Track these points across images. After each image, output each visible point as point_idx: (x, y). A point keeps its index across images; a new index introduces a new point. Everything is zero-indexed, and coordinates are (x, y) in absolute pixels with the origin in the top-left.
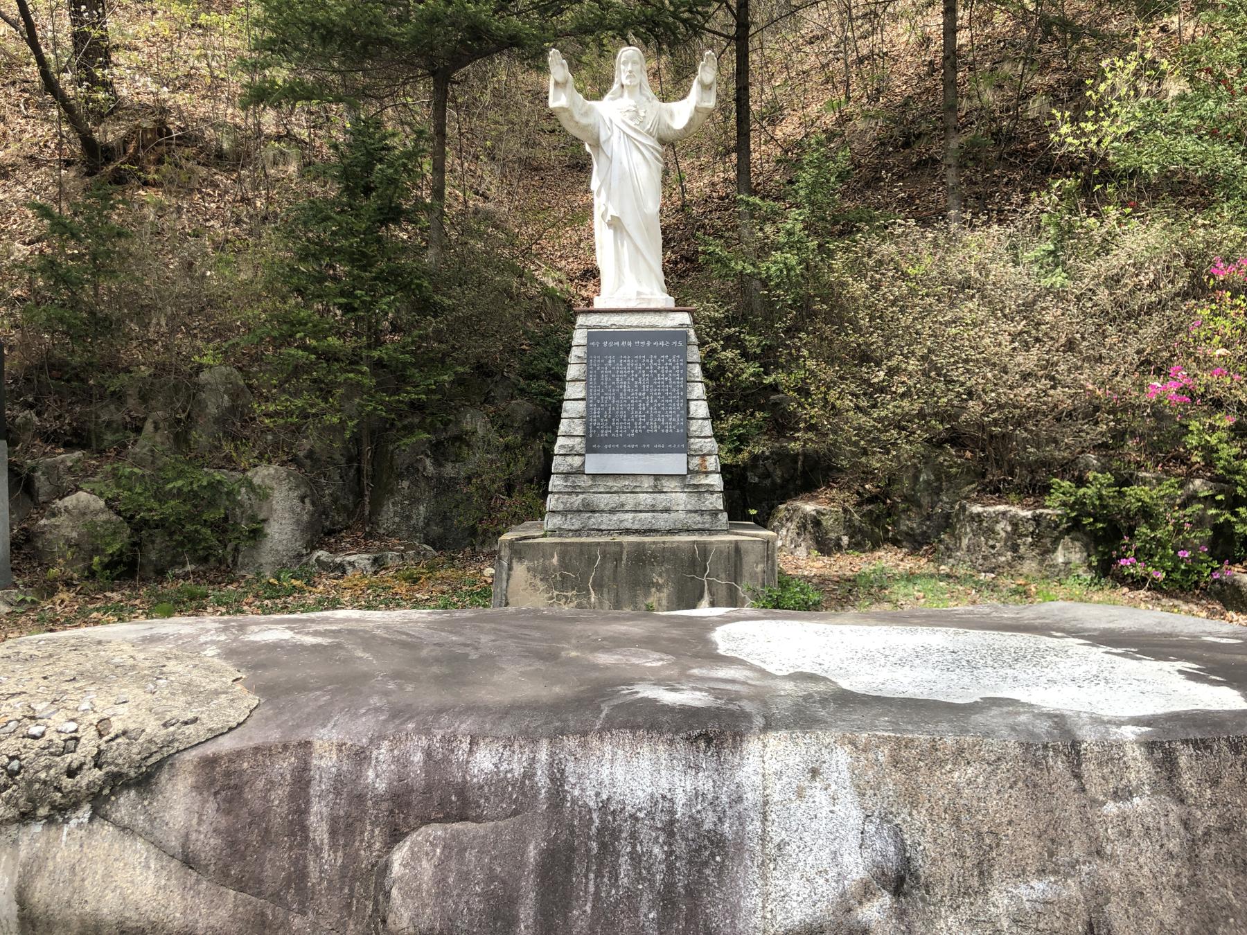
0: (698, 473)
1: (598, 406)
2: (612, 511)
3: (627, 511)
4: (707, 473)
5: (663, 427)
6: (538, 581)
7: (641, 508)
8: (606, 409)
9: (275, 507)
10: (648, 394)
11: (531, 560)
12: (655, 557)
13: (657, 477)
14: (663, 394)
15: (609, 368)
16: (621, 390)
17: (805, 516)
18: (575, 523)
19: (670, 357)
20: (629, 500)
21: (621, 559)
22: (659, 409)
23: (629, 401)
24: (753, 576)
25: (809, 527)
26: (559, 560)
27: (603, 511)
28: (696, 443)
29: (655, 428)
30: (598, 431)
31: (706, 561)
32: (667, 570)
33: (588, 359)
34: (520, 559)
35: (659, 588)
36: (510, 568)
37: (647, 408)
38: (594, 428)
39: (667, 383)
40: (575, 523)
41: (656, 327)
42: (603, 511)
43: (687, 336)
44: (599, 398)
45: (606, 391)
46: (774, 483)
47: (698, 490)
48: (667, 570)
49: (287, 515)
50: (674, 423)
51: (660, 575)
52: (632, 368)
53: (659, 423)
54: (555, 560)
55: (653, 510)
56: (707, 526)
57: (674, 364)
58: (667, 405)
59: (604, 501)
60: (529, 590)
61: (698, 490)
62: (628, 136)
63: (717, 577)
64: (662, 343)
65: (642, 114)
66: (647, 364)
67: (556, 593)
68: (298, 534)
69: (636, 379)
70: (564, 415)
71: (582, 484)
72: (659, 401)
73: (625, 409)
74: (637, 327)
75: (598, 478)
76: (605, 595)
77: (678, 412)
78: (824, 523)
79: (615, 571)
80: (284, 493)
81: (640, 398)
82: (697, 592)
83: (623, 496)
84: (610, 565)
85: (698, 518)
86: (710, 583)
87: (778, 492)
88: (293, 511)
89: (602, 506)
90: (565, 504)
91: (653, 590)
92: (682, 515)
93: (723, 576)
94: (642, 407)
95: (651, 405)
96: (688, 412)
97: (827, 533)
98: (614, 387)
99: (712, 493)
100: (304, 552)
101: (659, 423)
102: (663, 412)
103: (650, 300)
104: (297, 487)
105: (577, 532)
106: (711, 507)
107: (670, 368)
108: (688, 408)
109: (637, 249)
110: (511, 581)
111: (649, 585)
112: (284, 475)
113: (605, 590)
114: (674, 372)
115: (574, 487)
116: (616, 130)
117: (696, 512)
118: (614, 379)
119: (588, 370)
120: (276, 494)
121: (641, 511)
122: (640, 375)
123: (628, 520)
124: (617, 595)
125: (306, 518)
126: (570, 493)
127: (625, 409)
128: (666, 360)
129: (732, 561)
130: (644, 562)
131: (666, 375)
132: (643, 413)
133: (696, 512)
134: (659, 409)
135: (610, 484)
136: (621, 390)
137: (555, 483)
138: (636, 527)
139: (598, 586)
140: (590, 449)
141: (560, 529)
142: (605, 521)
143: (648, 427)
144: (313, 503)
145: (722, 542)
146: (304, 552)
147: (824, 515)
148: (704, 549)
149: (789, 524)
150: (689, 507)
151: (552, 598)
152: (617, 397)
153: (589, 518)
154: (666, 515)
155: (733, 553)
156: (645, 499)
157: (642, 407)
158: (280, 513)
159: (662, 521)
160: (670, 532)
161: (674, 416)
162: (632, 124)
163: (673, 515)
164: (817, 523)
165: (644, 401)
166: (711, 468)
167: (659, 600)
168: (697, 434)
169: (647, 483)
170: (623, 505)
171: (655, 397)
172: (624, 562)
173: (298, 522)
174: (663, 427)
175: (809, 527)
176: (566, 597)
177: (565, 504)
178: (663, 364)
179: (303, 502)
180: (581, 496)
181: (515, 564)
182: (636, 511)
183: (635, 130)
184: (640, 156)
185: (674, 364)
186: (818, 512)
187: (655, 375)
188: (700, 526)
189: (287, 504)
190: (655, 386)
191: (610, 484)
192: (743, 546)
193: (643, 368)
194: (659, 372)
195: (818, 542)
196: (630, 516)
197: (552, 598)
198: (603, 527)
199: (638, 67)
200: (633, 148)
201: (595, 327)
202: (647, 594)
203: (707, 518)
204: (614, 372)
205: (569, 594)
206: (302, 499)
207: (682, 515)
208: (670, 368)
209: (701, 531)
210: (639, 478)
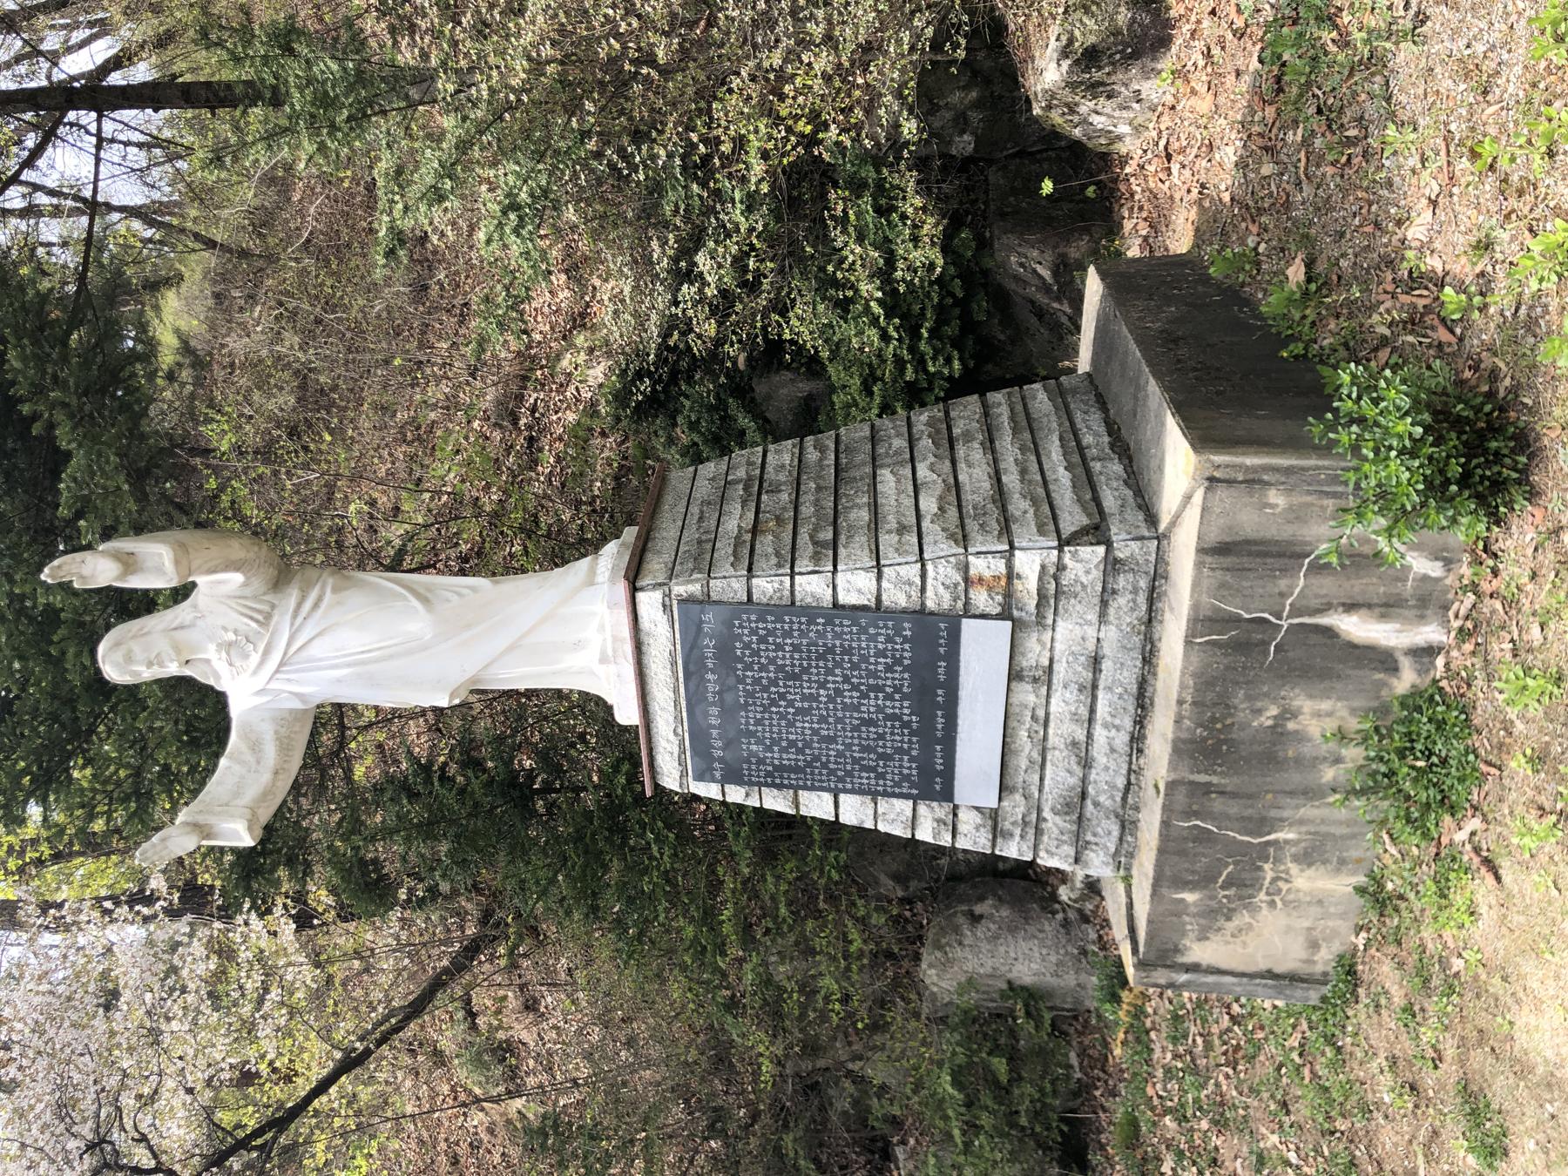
0: (1008, 594)
1: (849, 774)
2: (1086, 763)
3: (1089, 736)
4: (1011, 575)
5: (898, 661)
6: (1230, 926)
7: (1084, 712)
8: (855, 761)
9: (989, 970)
10: (822, 685)
11: (1184, 934)
12: (1213, 720)
13: (1014, 675)
14: (821, 657)
15: (769, 749)
16: (815, 732)
17: (1071, 85)
18: (1106, 831)
19: (739, 637)
20: (1062, 730)
21: (1209, 784)
22: (855, 666)
23: (839, 720)
24: (1296, 515)
25: (1097, 75)
26: (1191, 890)
27: (1084, 780)
28: (938, 598)
29: (905, 679)
30: (907, 778)
31: (1238, 620)
32: (1249, 698)
33: (751, 784)
34: (1177, 950)
35: (1289, 713)
36: (1194, 968)
37: (855, 688)
38: (898, 784)
39: (796, 648)
40: (1106, 831)
41: (673, 655)
42: (1084, 780)
43: (685, 601)
44: (832, 772)
45: (816, 758)
46: (977, 105)
47: (1053, 593)
48: (1249, 698)
49: (1002, 949)
50: (889, 639)
51: (1259, 712)
52: (766, 709)
53: (889, 668)
54: (1190, 897)
55: (1092, 689)
56: (1143, 583)
57: (753, 632)
58: (847, 651)
59: (1060, 776)
60: (1249, 938)
61: (1053, 593)
62: (282, 664)
63: (1283, 595)
64: (941, 670)
65: (231, 636)
66: (757, 681)
67: (1262, 896)
68: (1031, 929)
69: (791, 704)
70: (869, 825)
71: (1020, 811)
72: (838, 665)
73: (855, 729)
74: (676, 691)
75: (1009, 782)
76: (1285, 814)
77: (863, 630)
78: (1092, 39)
79: (1234, 795)
80: (967, 953)
81: (831, 699)
82: (1314, 639)
83: (1053, 740)
84: (1218, 804)
85: (1122, 601)
86: (1296, 611)
87: (997, 90)
88: (996, 937)
89: (1073, 781)
90: (1060, 843)
91: (1291, 726)
92: (1110, 634)
93: (1283, 584)
94: (850, 697)
95: (846, 679)
96: (864, 608)
97: (1117, 32)
98: (808, 745)
99: (1060, 567)
100: (1060, 916)
101: (889, 668)
102: (864, 659)
103: (615, 639)
104: (957, 930)
105: (1127, 826)
106: (1097, 574)
107: (762, 640)
108: (855, 608)
109: (511, 648)
110: (1224, 966)
111: (1278, 732)
112: (939, 954)
113: (1273, 813)
114: (771, 633)
115: (1025, 823)
116: (274, 685)
117: (1104, 604)
118: (792, 744)
119: (774, 785)
120: (969, 967)
121: (1092, 711)
122: (782, 696)
123: (1109, 739)
124: (1291, 793)
125: (1005, 912)
126: (1039, 832)
127: (855, 729)
128: (747, 646)
129: (1246, 561)
130: (1221, 742)
131: (779, 647)
132: (865, 696)
133: (1104, 604)
134: (855, 666)
135: (1024, 764)
136: (815, 732)
137: (1013, 850)
138: (1128, 723)
139: (1262, 825)
140: (947, 794)
141: (1117, 853)
142: (1107, 775)
143: (897, 689)
144: (981, 899)
145: (1196, 584)
146: (1060, 916)
147: (1071, 41)
148: (1201, 623)
149: (1083, 109)
150: (1092, 616)
151: (1272, 904)
152: (831, 740)
153: (1096, 804)
154: (1106, 665)
155: (1228, 561)
156: (1064, 702)
157: (850, 697)
158: (998, 962)
159: (1119, 674)
160: (1149, 658)
161: (873, 638)
162: (255, 658)
163: (1107, 650)
164: (1091, 57)
165: (838, 692)
166: (1000, 566)
167: (1318, 715)
168: (915, 594)
169: (1027, 695)
170: (1074, 744)
171: (829, 672)
172: (1215, 779)
173: (1013, 930)
174: (898, 661)
175: (1097, 75)
176: (1275, 880)
177: (1060, 843)
178: (756, 653)
179: (981, 917)
180: (1047, 814)
181: (1188, 958)
182: (1091, 721)
183: (267, 652)
184: (316, 643)
185: (753, 632)
186: (1065, 53)
187: (781, 668)
188: (1142, 599)
189: (985, 946)
190: (806, 670)
191: (1024, 764)
192: (1213, 537)
193: (765, 689)
194: (772, 661)
195: (1136, 55)
196: (1100, 733)
197: (1272, 904)
198: (1121, 782)
199: (136, 647)
200: (304, 654)
201: (682, 763)
202: (1300, 737)
203: (1122, 582)
204: (774, 742)
205: (1269, 875)
206: (975, 919)
207: (1110, 634)
208: (762, 640)
209: (1153, 597)
210: (1014, 709)
